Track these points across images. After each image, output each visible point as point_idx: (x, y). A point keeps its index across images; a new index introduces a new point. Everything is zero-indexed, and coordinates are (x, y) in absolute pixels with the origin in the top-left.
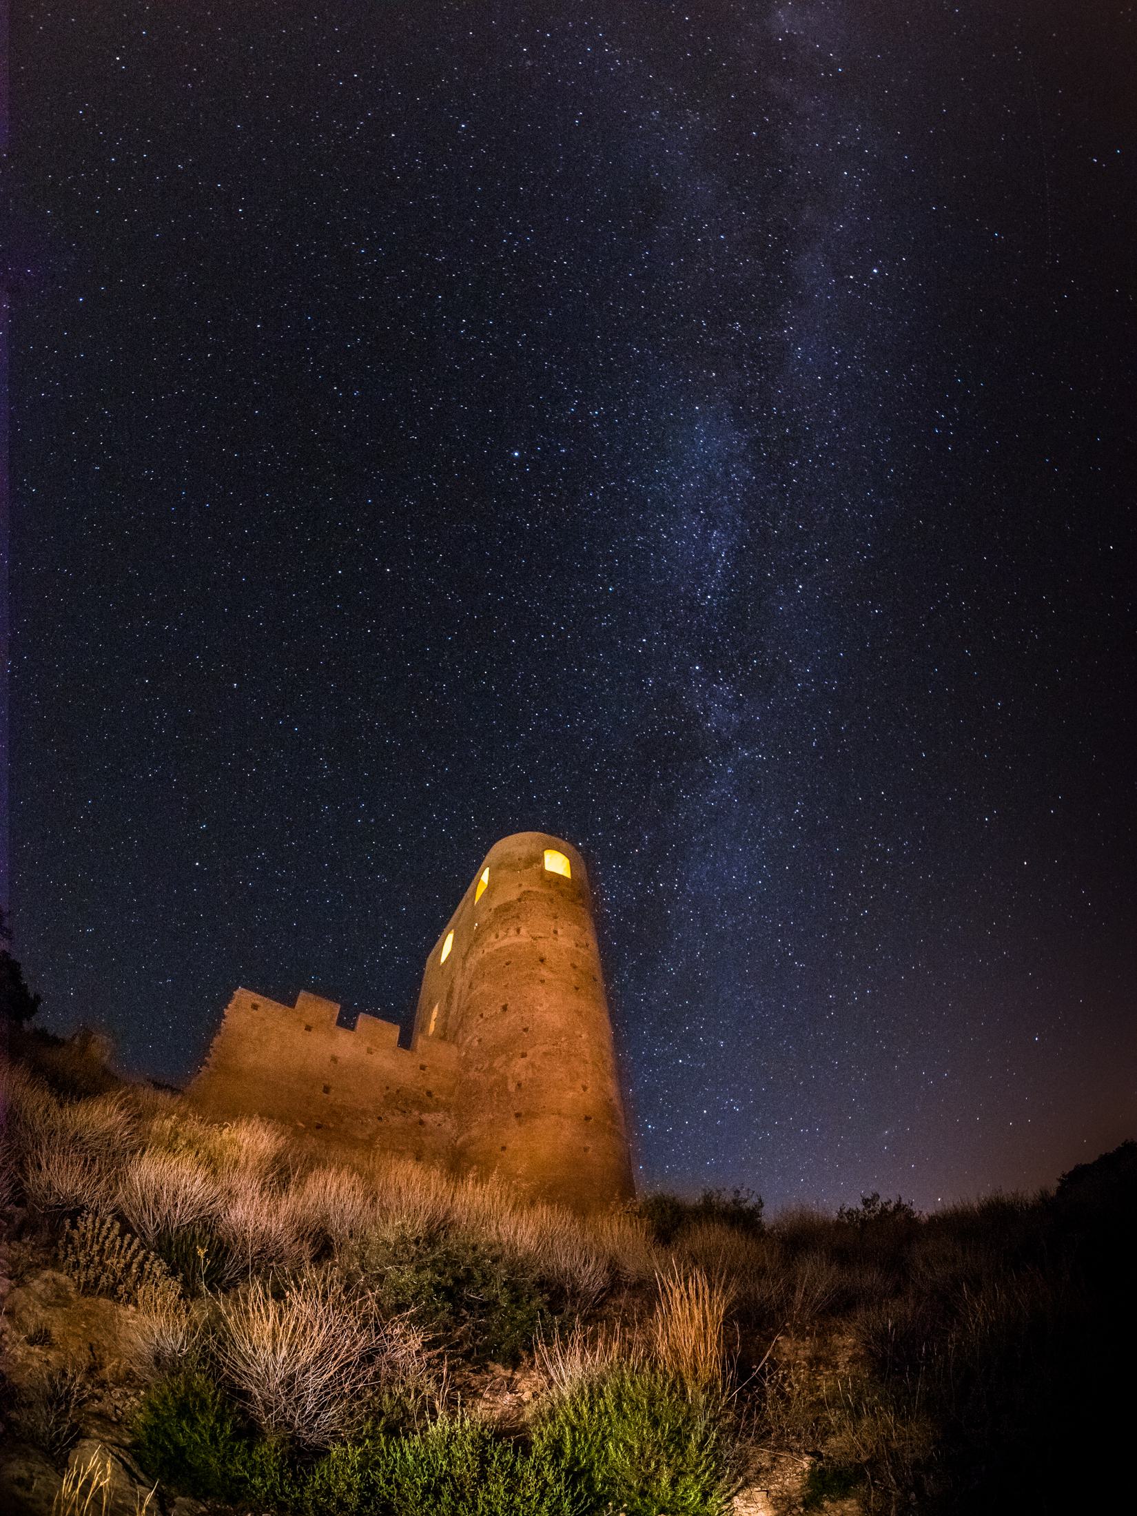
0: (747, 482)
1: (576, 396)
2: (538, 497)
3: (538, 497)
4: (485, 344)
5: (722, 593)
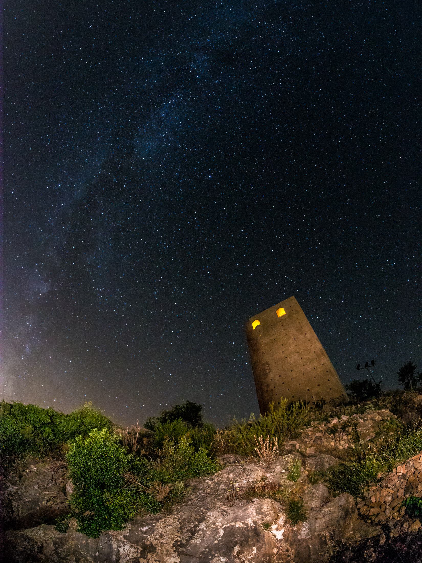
0: (142, 127)
1: (179, 183)
2: (213, 159)
3: (213, 159)
4: (195, 217)
5: (173, 95)
